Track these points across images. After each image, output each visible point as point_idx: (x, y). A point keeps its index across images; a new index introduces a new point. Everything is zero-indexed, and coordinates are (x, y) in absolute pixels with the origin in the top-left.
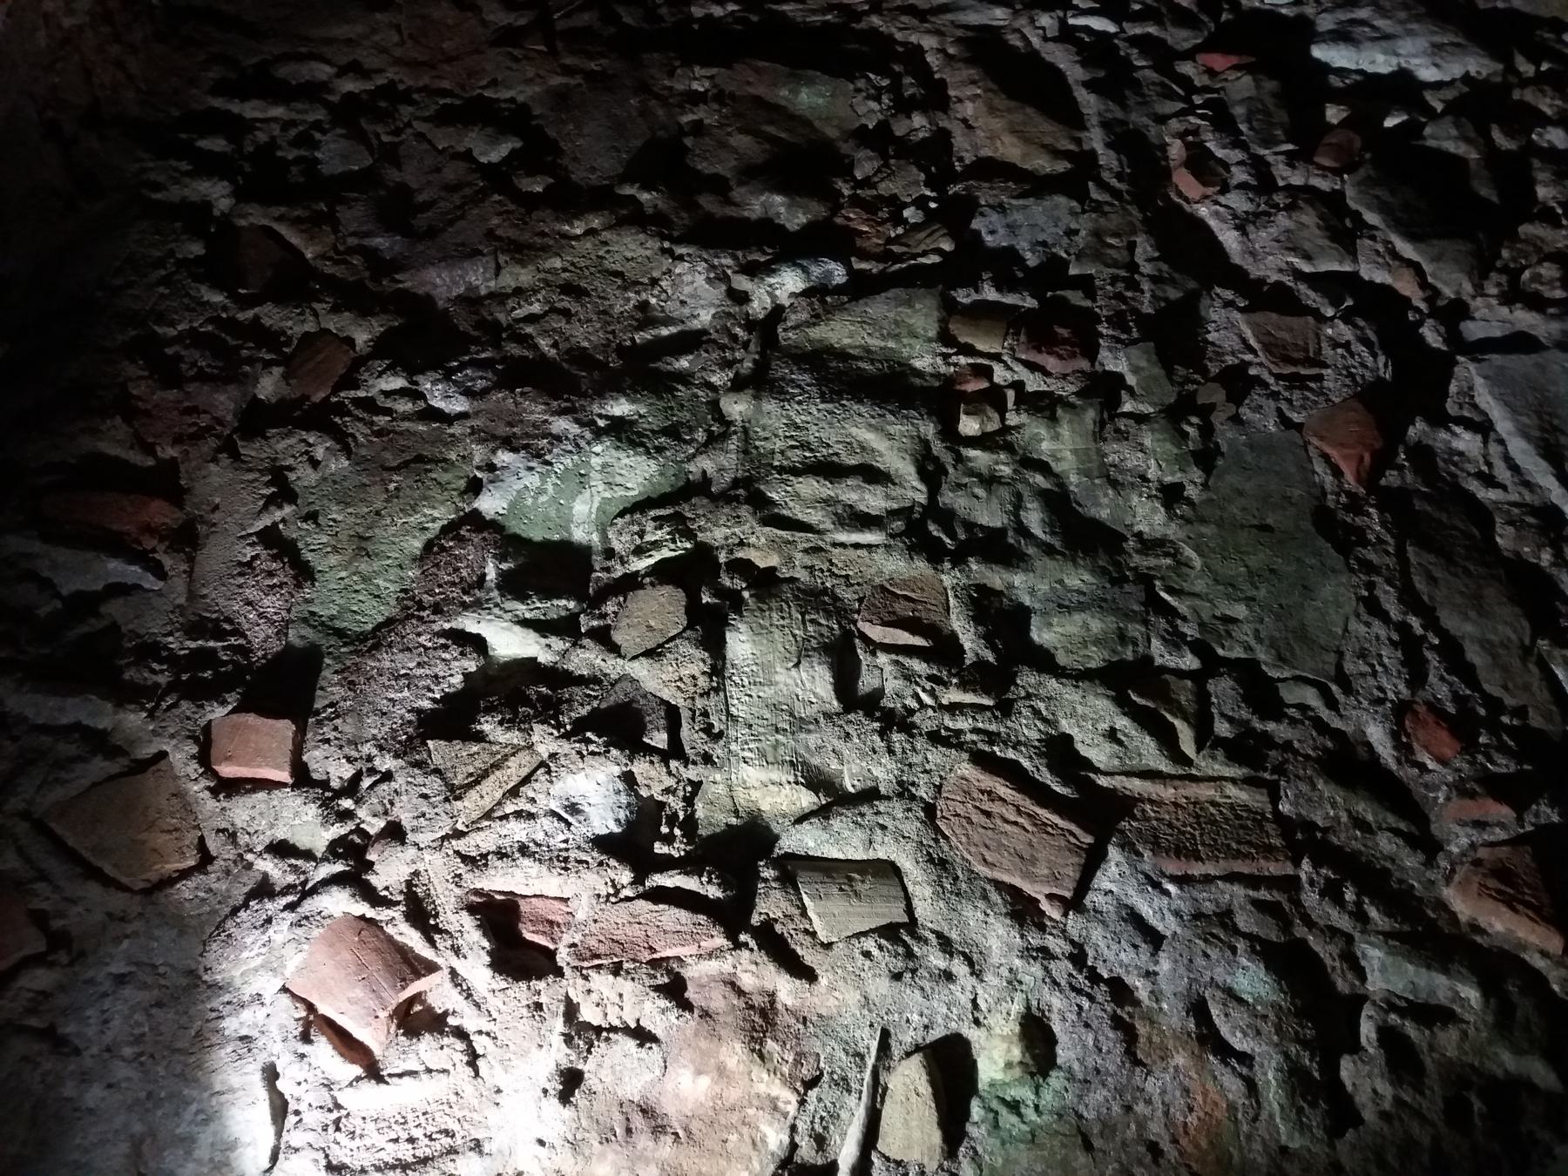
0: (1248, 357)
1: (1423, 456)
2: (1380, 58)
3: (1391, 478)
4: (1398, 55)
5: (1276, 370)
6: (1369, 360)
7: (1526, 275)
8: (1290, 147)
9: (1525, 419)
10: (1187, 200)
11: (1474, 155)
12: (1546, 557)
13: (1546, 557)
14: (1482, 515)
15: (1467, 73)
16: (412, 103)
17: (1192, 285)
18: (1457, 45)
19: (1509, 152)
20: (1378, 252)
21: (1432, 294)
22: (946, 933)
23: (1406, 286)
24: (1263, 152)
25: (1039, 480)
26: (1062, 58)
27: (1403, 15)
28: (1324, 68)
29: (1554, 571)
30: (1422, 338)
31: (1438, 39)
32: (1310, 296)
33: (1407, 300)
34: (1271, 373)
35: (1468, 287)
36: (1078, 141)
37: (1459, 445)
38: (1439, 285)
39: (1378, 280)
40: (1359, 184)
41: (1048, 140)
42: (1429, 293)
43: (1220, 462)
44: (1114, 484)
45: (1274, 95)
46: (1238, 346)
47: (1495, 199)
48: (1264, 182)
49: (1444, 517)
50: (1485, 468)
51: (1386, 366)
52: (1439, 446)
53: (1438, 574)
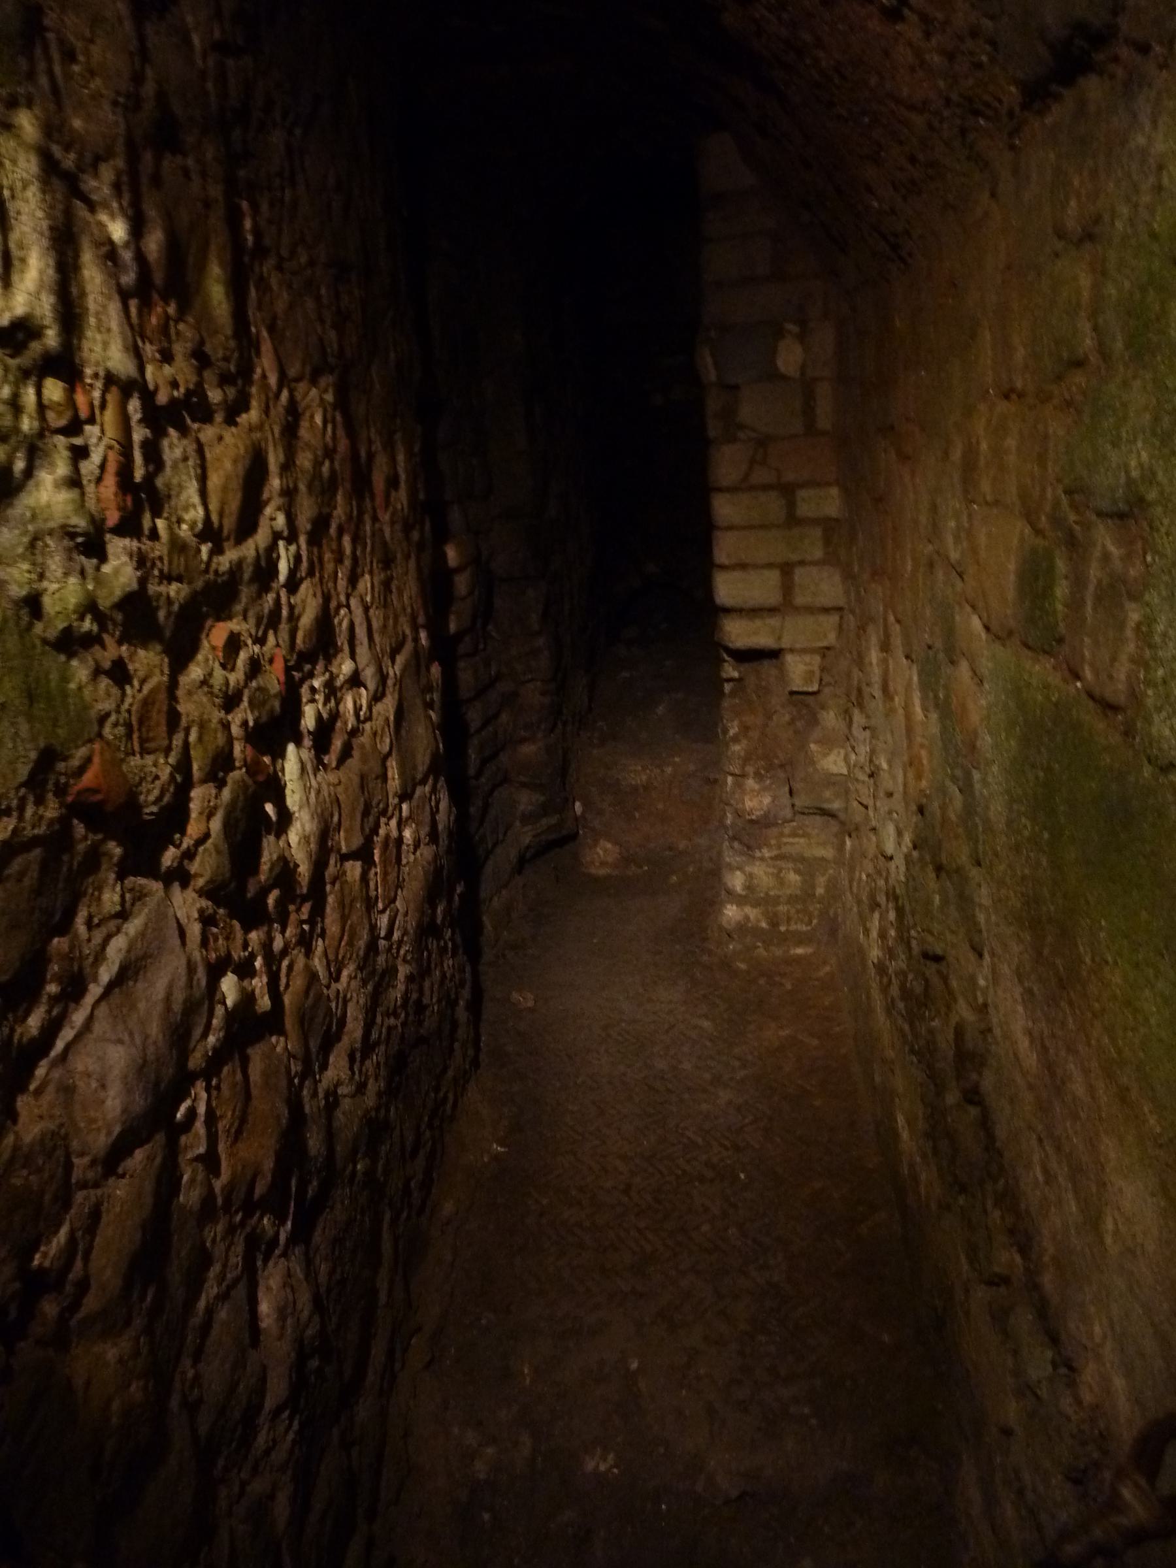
0: (136, 683)
1: (94, 859)
2: (297, 797)
3: (80, 829)
4: (299, 811)
5: (134, 708)
6: (151, 798)
7: (215, 930)
8: (251, 724)
9: (139, 945)
10: (208, 635)
11: (263, 878)
12: (52, 988)
13: (52, 988)
14: (65, 926)
15: (299, 866)
16: (56, 578)
17: (168, 633)
18: (311, 855)
19: (266, 904)
20: (209, 801)
21: (189, 855)
22: (105, 1219)
23: (194, 829)
24: (245, 699)
25: (20, 465)
26: (261, 538)
27: (319, 810)
28: (282, 755)
29: (44, 999)
30: (166, 848)
31: (312, 839)
32: (177, 740)
33: (183, 833)
34: (131, 705)
35: (200, 882)
36: (228, 539)
37: (106, 896)
38: (198, 859)
39: (192, 805)
40: (243, 780)
41: (227, 511)
42: (192, 848)
43: (63, 658)
44: (32, 545)
45: (272, 711)
46: (141, 674)
47: (249, 895)
48: (230, 701)
49: (61, 885)
50: (96, 921)
51: (152, 814)
52: (102, 874)
53: (27, 882)
